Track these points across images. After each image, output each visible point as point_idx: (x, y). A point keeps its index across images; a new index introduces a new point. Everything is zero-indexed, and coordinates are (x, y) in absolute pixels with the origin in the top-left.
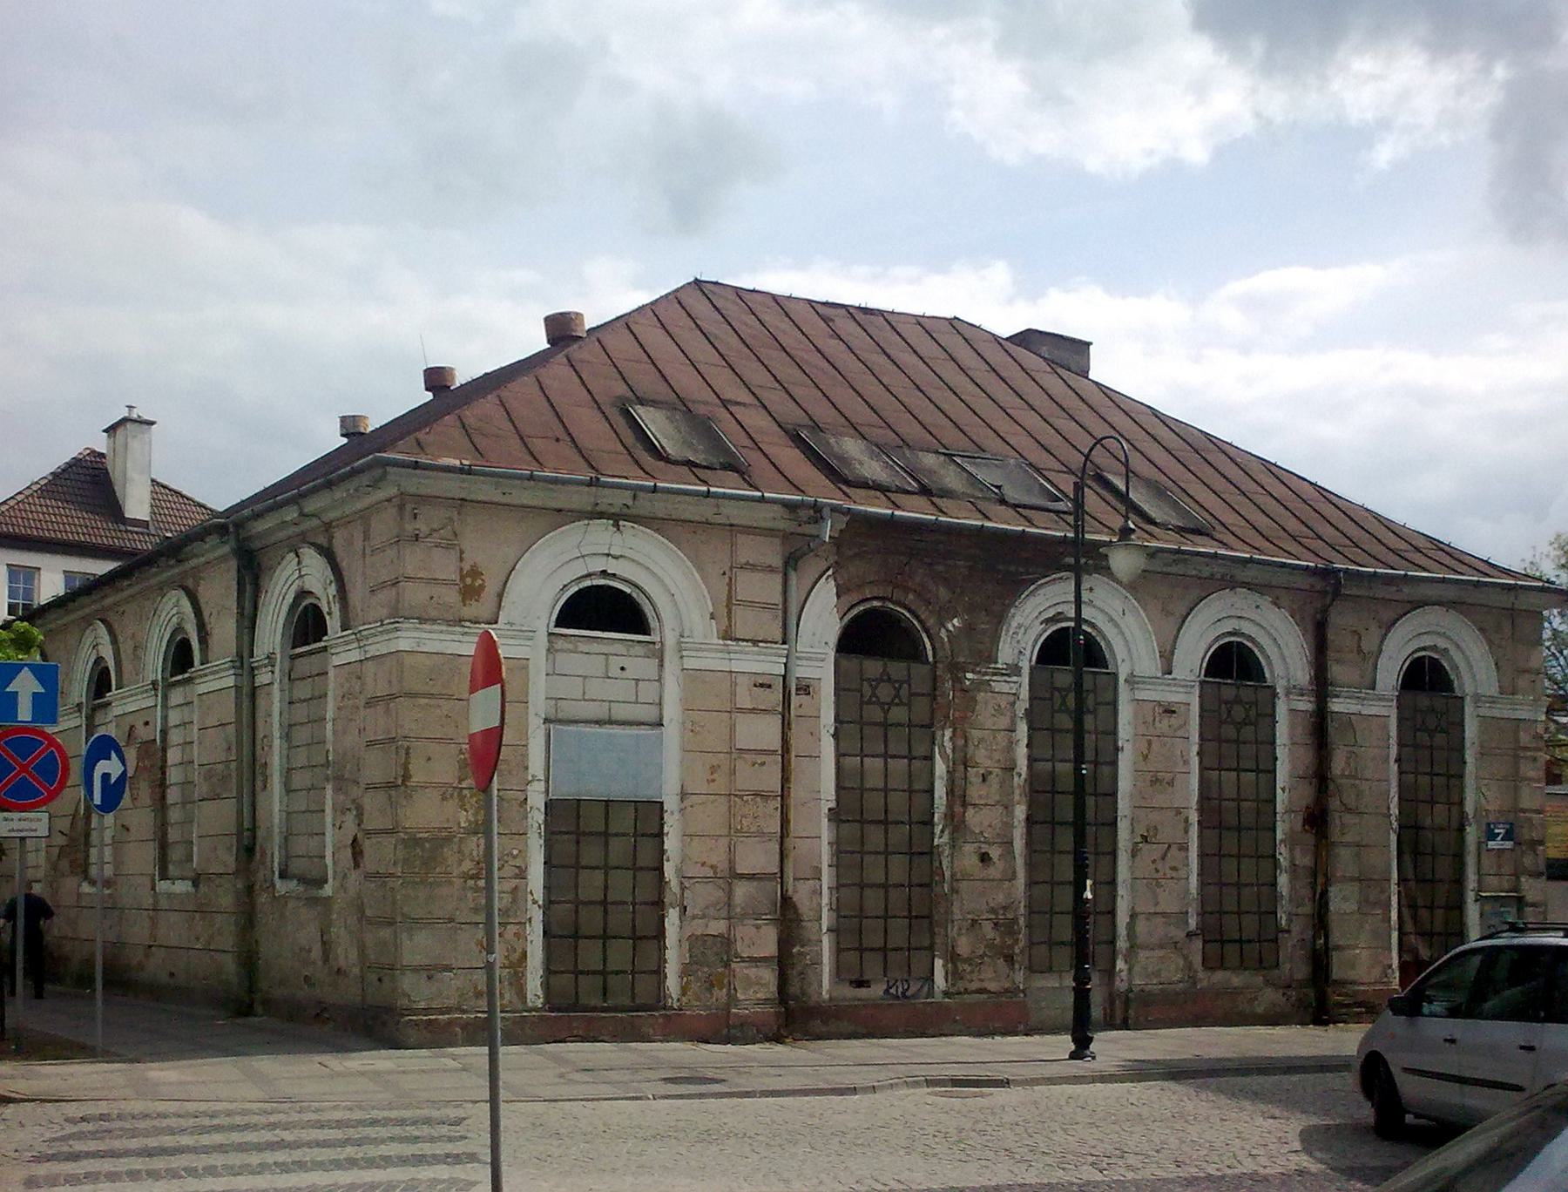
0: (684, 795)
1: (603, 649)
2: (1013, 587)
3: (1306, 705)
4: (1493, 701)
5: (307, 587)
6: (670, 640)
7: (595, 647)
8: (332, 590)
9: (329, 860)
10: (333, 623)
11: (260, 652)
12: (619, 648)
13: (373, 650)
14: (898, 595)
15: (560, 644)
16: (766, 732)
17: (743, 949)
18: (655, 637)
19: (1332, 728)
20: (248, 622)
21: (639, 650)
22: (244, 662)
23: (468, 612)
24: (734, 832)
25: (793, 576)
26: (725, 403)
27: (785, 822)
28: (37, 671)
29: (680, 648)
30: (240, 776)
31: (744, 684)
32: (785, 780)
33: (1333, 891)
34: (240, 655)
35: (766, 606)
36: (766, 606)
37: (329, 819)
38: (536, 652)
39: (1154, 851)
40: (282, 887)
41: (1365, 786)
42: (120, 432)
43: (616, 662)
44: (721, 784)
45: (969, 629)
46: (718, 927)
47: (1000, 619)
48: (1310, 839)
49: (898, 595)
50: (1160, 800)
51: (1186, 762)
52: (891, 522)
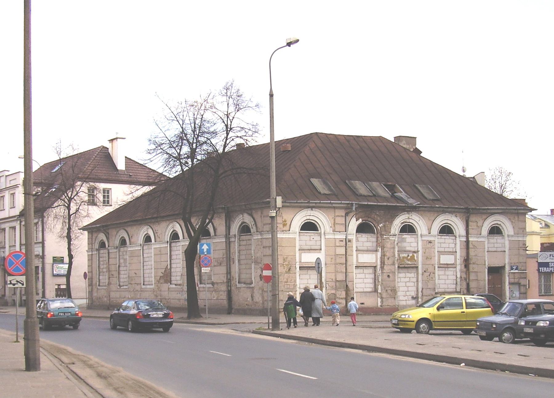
0: (326, 264)
1: (309, 235)
2: (393, 217)
3: (464, 239)
4: (512, 236)
5: (245, 221)
6: (323, 233)
7: (308, 234)
8: (253, 223)
9: (253, 279)
10: (253, 230)
11: (232, 233)
12: (313, 234)
13: (265, 237)
14: (369, 219)
15: (301, 234)
16: (342, 251)
17: (338, 296)
18: (319, 232)
19: (471, 246)
20: (228, 228)
21: (316, 234)
22: (227, 236)
23: (284, 229)
24: (336, 272)
25: (347, 217)
26: (328, 174)
27: (346, 269)
28: (207, 245)
29: (325, 234)
30: (227, 261)
31: (337, 241)
32: (346, 260)
33: (470, 283)
34: (226, 235)
35: (342, 224)
36: (342, 224)
37: (253, 271)
38: (297, 236)
39: (427, 274)
40: (238, 285)
41: (479, 258)
42: (115, 141)
43: (312, 237)
44: (333, 262)
45: (384, 226)
46: (333, 292)
47: (391, 223)
48: (465, 270)
49: (369, 219)
50: (428, 262)
51: (435, 253)
52: (367, 205)
